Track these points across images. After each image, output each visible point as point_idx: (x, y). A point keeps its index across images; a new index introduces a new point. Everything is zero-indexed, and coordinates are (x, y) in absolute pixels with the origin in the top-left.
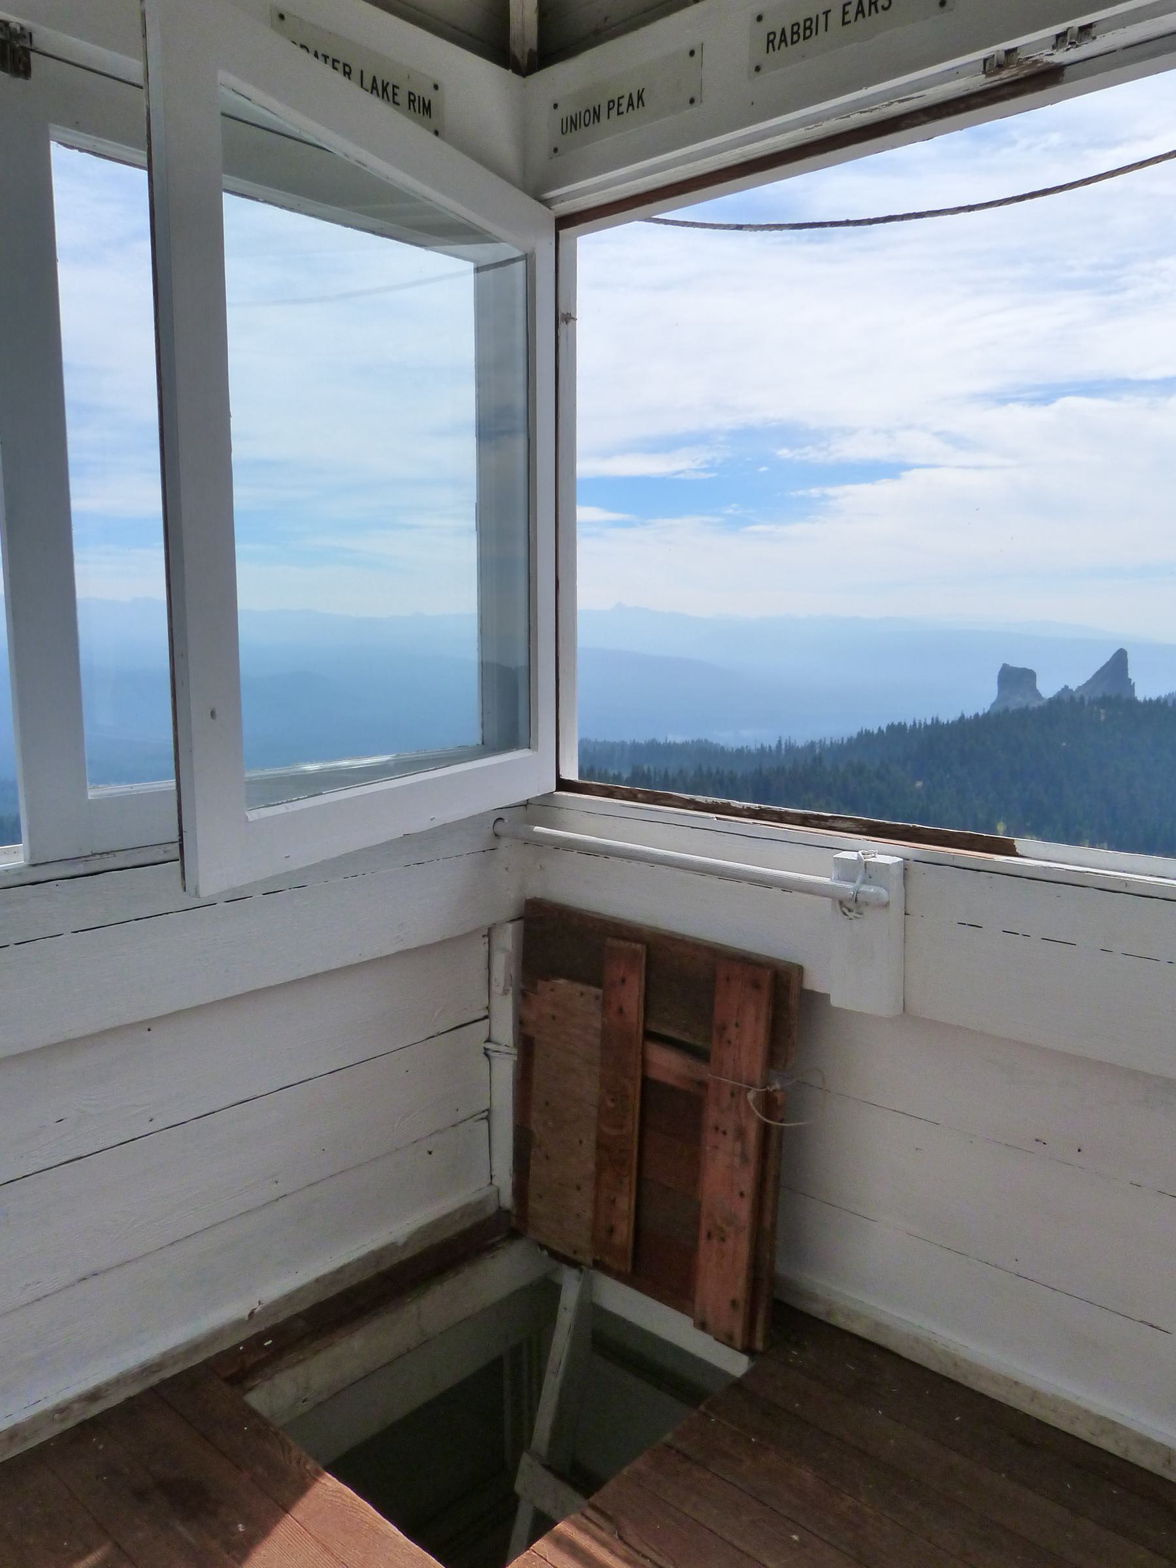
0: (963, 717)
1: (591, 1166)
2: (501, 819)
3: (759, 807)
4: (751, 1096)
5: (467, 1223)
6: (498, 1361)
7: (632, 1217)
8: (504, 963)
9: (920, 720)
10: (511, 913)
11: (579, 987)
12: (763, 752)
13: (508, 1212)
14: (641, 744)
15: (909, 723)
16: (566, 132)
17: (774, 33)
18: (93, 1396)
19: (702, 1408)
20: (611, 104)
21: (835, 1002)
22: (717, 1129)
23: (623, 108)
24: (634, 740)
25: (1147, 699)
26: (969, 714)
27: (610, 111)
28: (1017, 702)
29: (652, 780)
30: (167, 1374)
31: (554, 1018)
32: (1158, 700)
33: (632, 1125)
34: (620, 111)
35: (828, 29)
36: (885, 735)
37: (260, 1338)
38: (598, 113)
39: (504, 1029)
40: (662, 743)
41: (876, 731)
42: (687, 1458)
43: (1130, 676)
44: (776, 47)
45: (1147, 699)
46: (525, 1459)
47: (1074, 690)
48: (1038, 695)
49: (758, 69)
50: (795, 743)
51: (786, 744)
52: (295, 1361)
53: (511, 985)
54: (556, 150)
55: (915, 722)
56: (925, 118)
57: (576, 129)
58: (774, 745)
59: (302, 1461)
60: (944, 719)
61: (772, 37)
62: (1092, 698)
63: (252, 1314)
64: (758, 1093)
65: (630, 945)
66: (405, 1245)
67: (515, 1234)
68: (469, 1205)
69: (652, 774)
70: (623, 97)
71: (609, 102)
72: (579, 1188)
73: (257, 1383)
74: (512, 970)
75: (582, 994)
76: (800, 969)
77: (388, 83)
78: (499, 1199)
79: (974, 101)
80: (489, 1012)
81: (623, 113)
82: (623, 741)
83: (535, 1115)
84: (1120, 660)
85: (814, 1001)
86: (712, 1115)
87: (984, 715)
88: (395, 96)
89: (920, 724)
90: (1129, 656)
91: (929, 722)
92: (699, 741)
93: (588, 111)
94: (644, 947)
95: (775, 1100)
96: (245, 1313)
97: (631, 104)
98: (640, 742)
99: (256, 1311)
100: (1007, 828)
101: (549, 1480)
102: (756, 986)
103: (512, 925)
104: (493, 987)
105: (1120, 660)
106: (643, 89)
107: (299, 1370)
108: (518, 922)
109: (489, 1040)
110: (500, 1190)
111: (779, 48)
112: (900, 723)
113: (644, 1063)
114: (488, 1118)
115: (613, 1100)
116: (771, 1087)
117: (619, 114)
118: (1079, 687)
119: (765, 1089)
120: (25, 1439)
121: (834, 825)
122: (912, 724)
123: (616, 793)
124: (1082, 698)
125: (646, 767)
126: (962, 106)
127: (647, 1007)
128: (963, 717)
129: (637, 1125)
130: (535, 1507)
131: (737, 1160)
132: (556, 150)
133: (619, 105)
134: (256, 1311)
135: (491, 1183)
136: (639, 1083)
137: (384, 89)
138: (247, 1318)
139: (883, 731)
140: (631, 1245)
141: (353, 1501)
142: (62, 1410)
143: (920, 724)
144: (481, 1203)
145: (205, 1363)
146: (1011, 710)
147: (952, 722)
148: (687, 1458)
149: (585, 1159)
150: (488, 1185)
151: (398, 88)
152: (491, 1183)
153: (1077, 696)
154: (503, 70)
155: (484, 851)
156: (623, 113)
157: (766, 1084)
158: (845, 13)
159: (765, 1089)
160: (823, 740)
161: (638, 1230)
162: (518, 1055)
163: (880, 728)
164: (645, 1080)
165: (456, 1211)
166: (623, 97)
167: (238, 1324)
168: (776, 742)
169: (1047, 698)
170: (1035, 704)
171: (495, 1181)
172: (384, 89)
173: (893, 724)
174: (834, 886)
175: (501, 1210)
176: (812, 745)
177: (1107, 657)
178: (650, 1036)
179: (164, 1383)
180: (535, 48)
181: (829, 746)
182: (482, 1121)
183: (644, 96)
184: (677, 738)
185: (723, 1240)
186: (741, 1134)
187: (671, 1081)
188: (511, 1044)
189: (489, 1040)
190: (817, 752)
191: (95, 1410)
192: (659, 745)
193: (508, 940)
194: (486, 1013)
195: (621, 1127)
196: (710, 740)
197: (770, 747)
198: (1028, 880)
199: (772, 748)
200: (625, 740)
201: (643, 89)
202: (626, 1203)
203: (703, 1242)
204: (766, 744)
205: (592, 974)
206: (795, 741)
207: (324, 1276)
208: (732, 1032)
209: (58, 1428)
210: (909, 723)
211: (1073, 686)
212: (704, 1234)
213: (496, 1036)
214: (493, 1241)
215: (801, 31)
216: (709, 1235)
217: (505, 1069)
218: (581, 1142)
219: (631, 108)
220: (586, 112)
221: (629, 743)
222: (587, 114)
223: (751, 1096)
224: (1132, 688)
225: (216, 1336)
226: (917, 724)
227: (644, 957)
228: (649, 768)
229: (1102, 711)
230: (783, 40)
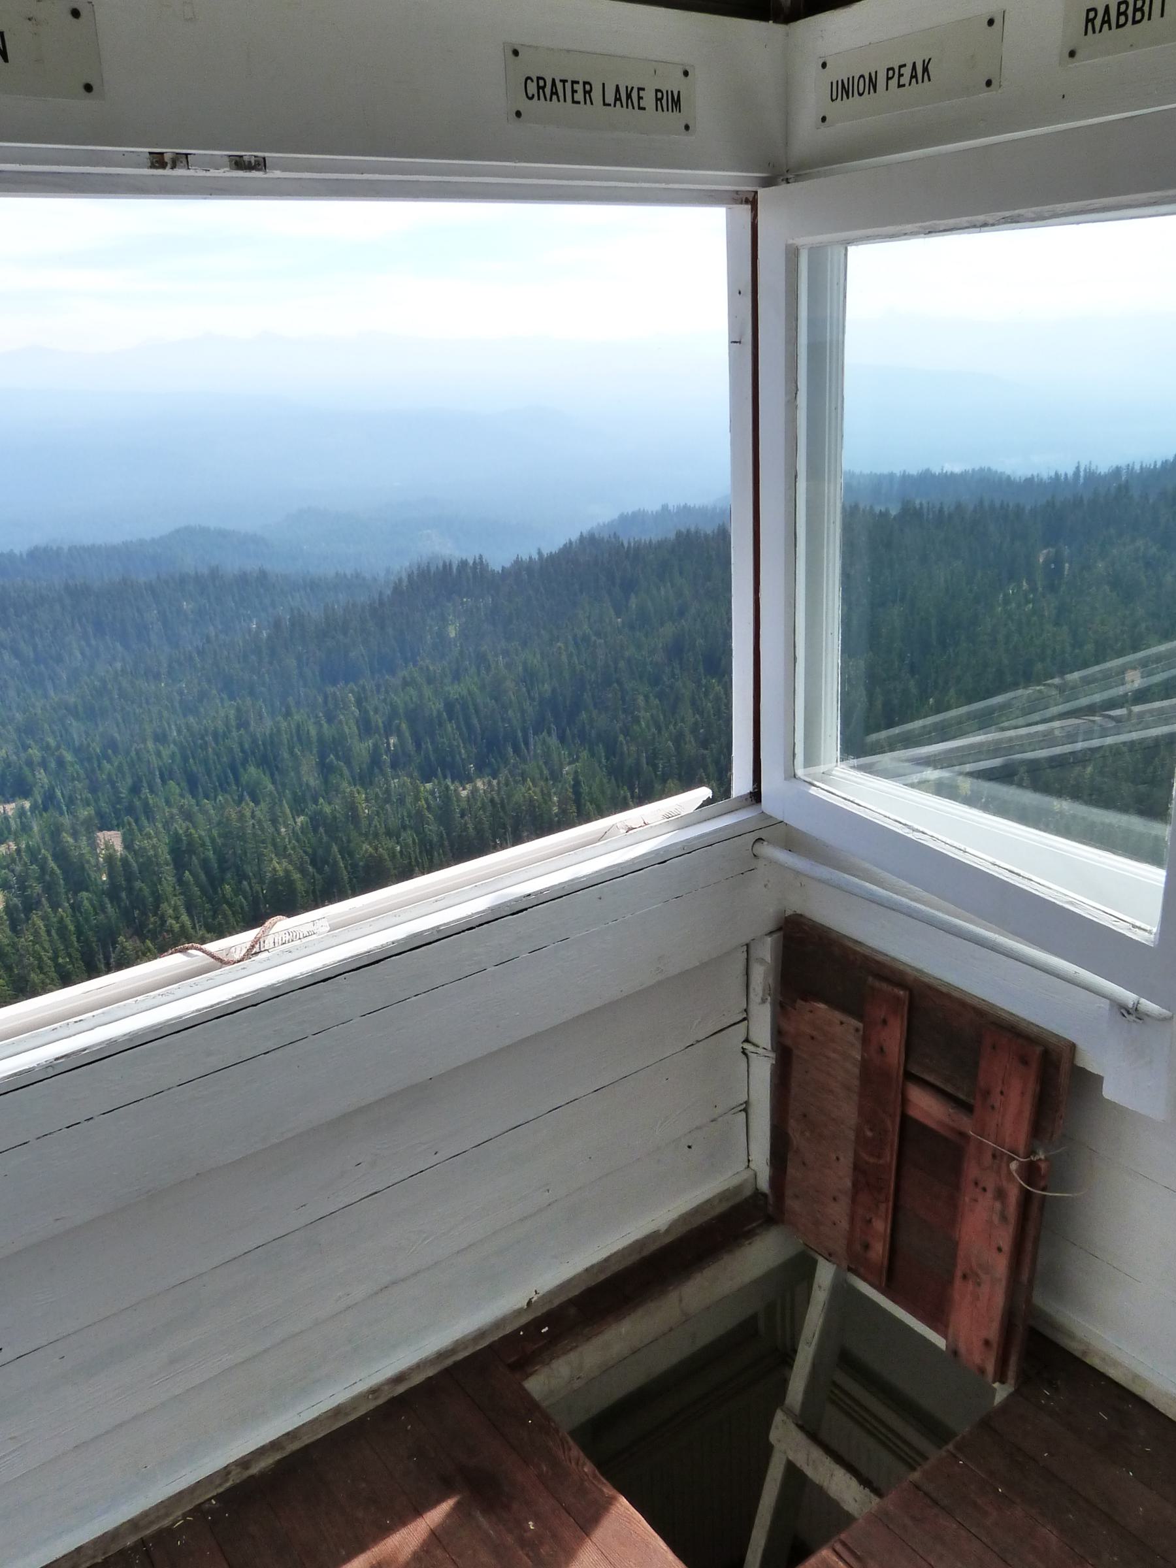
1: (848, 1183)
2: (761, 839)
4: (1014, 1166)
5: (724, 1207)
6: (754, 1318)
7: (888, 1239)
8: (761, 976)
10: (771, 926)
11: (838, 1016)
12: (1057, 481)
13: (764, 1195)
14: (913, 476)
16: (836, 99)
17: (1094, 10)
18: (399, 1379)
19: (950, 1447)
20: (891, 73)
21: (1109, 1092)
22: (976, 1184)
23: (905, 80)
24: (905, 471)
27: (890, 81)
29: (925, 517)
30: (460, 1356)
31: (812, 1038)
33: (889, 1157)
35: (1165, 14)
37: (537, 1323)
38: (874, 80)
39: (762, 1028)
40: (937, 474)
42: (936, 1503)
44: (1097, 28)
46: (779, 1416)
49: (1072, 54)
50: (1097, 469)
51: (1085, 469)
52: (569, 1347)
53: (769, 995)
54: (824, 119)
57: (848, 98)
58: (1070, 473)
59: (581, 1462)
61: (1092, 15)
63: (529, 1303)
64: (1021, 1164)
65: (893, 990)
66: (667, 1231)
67: (771, 1220)
68: (728, 1190)
69: (925, 510)
70: (904, 65)
71: (888, 70)
72: (835, 1199)
73: (536, 1368)
74: (771, 981)
75: (842, 1023)
76: (1073, 1047)
77: (632, 88)
78: (756, 1182)
80: (747, 1014)
81: (904, 85)
82: (892, 473)
83: (792, 1123)
85: (1087, 1082)
86: (972, 1171)
88: (641, 101)
92: (982, 470)
93: (860, 95)
94: (907, 993)
95: (1039, 1169)
96: (524, 1304)
97: (914, 76)
98: (911, 473)
99: (533, 1300)
101: (799, 1437)
102: (1024, 1061)
103: (769, 939)
104: (752, 995)
106: (930, 59)
107: (573, 1356)
108: (775, 936)
109: (747, 1041)
110: (758, 1174)
111: (1100, 31)
113: (905, 1101)
114: (745, 1110)
115: (871, 1130)
116: (1034, 1156)
117: (900, 86)
119: (1028, 1159)
120: (347, 1414)
125: (917, 502)
127: (909, 1048)
129: (895, 1157)
130: (787, 1458)
131: (996, 1219)
132: (824, 119)
133: (901, 75)
134: (533, 1300)
135: (748, 1166)
136: (898, 1119)
137: (629, 96)
138: (526, 1307)
140: (886, 1262)
141: (627, 1511)
142: (375, 1391)
144: (738, 1189)
145: (490, 1346)
148: (936, 1503)
149: (840, 1176)
150: (745, 1168)
151: (643, 89)
152: (748, 1166)
155: (742, 874)
156: (904, 85)
157: (1031, 1152)
159: (1028, 1159)
160: (1131, 465)
161: (893, 1250)
162: (776, 1060)
164: (905, 1119)
165: (714, 1197)
166: (904, 65)
167: (519, 1313)
168: (1074, 469)
171: (752, 1165)
172: (629, 96)
175: (757, 1194)
176: (1117, 471)
178: (909, 1076)
179: (457, 1365)
181: (1138, 471)
182: (740, 1113)
184: (957, 468)
185: (979, 1284)
186: (1001, 1194)
187: (933, 1125)
188: (769, 1047)
189: (747, 1041)
190: (1123, 479)
191: (401, 1389)
192: (933, 476)
193: (766, 951)
194: (745, 1016)
195: (879, 1157)
196: (994, 467)
197: (1066, 475)
199: (1069, 476)
200: (894, 472)
201: (930, 59)
202: (881, 1226)
203: (958, 1282)
204: (1062, 472)
205: (853, 1005)
206: (1097, 467)
207: (592, 1266)
208: (996, 1099)
209: (372, 1405)
212: (959, 1274)
213: (754, 1037)
214: (750, 1227)
215: (1130, 12)
216: (965, 1277)
217: (763, 1069)
218: (838, 1159)
219: (914, 80)
220: (860, 78)
221: (898, 475)
222: (862, 80)
223: (1014, 1166)
225: (498, 1324)
227: (907, 1003)
228: (921, 504)
230: (1106, 21)
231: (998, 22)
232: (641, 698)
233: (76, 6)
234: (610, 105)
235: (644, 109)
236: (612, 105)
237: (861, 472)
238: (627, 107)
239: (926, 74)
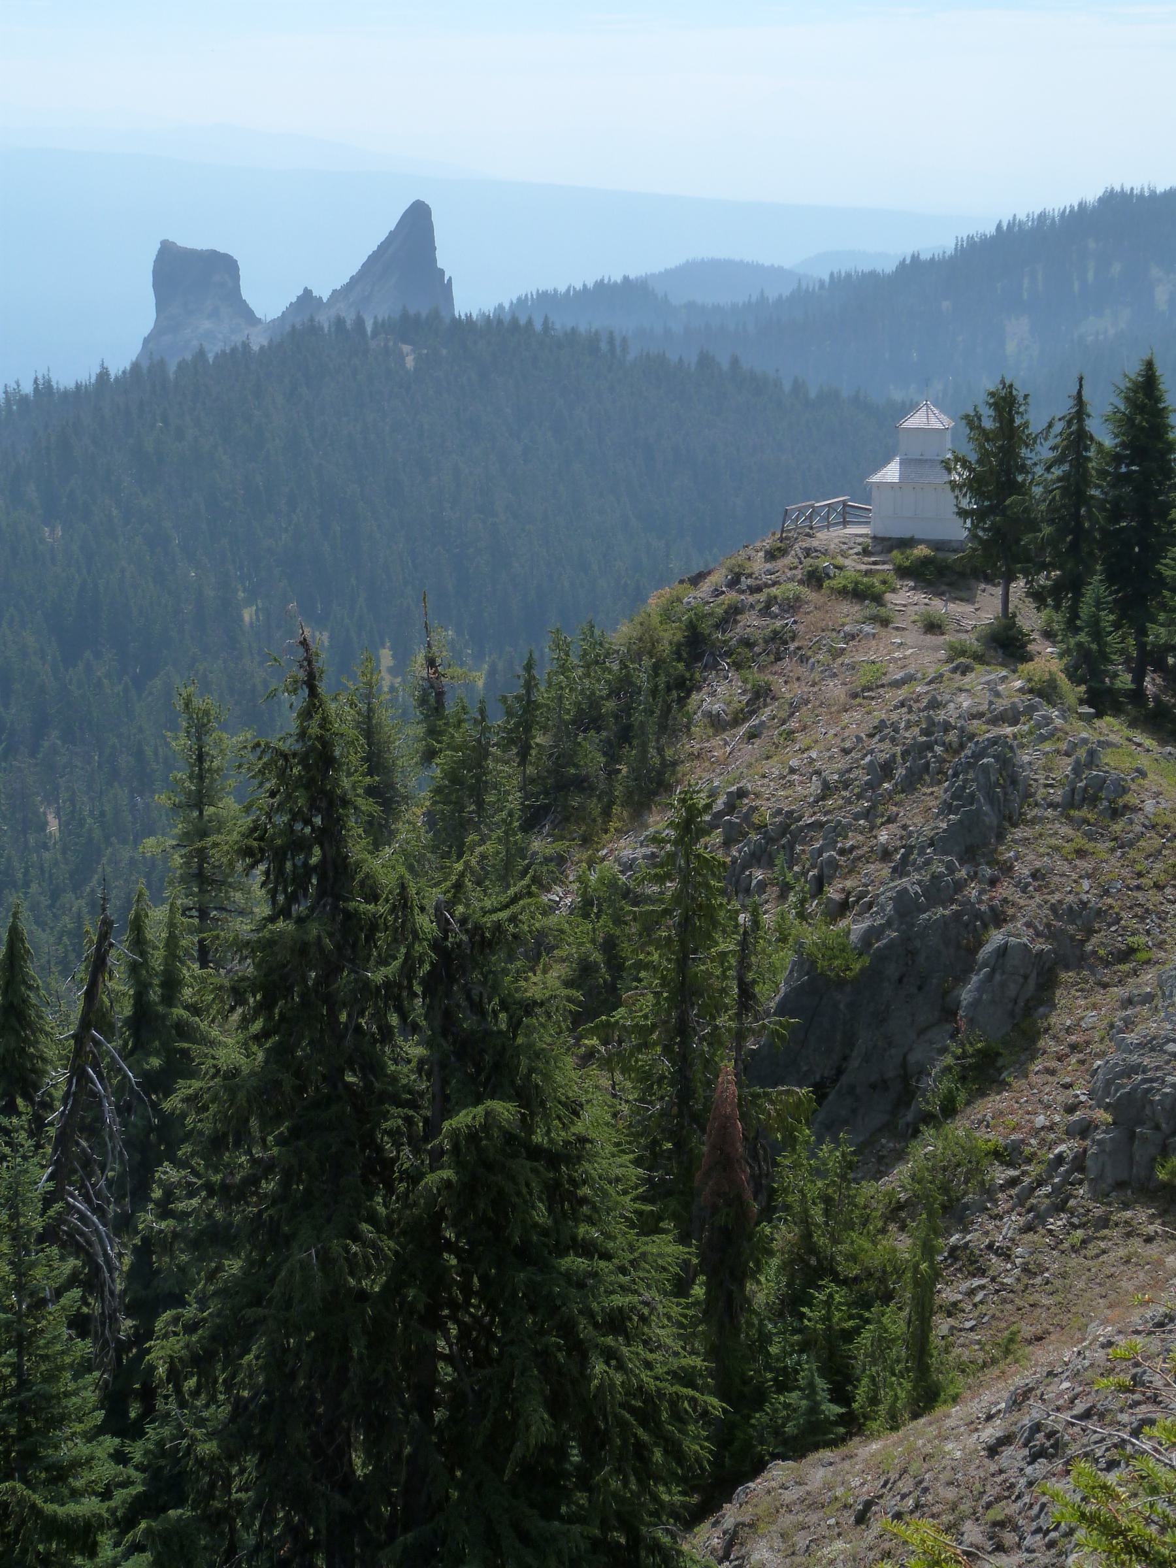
0: (103, 375)
43: (440, 265)
47: (325, 300)
62: (380, 319)
90: (435, 218)
91: (27, 388)
118: (335, 291)
169: (268, 320)
170: (258, 341)
197: (1132, 189)
224: (445, 289)
229: (406, 348)
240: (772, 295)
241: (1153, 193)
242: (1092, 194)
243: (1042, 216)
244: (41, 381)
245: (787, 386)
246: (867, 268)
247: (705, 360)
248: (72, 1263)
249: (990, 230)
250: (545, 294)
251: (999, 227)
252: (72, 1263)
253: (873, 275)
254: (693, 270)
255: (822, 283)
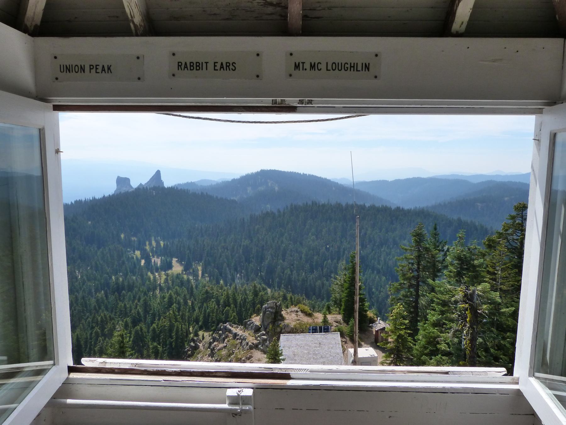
0: (104, 196)
3: (180, 370)
9: (88, 198)
15: (83, 200)
25: (168, 187)
26: (107, 195)
27: (91, 70)
28: (124, 190)
32: (172, 187)
34: (97, 71)
36: (74, 205)
41: (70, 204)
44: (183, 69)
45: (168, 187)
48: (132, 187)
55: (85, 199)
56: (244, 110)
60: (97, 197)
62: (150, 187)
79: (263, 109)
84: (158, 173)
87: (112, 195)
89: (88, 199)
90: (161, 172)
91: (91, 199)
100: (125, 236)
105: (158, 173)
112: (79, 200)
118: (145, 184)
121: (216, 375)
122: (85, 200)
123: (102, 370)
124: (147, 187)
126: (259, 109)
128: (104, 196)
139: (73, 203)
143: (88, 199)
146: (122, 193)
147: (100, 198)
153: (145, 187)
154: (24, 34)
158: (215, 66)
163: (71, 202)
169: (135, 187)
170: (131, 190)
173: (77, 200)
174: (231, 409)
177: (153, 173)
180: (39, 23)
183: (111, 68)
198: (300, 390)
210: (83, 200)
211: (143, 183)
226: (87, 200)
229: (154, 192)
231: (141, 59)
232: (112, 341)
233: (56, 60)
234: (359, 71)
235: (321, 69)
236: (361, 70)
237: (390, 207)
238: (226, 70)
239: (109, 70)
240: (213, 184)
241: (268, 170)
242: (259, 170)
243: (252, 173)
244: (93, 197)
245: (215, 197)
246: (227, 180)
247: (202, 193)
248: (447, 252)
249: (245, 175)
250: (179, 184)
251: (246, 174)
252: (447, 252)
253: (228, 181)
254: (202, 181)
255: (220, 182)
